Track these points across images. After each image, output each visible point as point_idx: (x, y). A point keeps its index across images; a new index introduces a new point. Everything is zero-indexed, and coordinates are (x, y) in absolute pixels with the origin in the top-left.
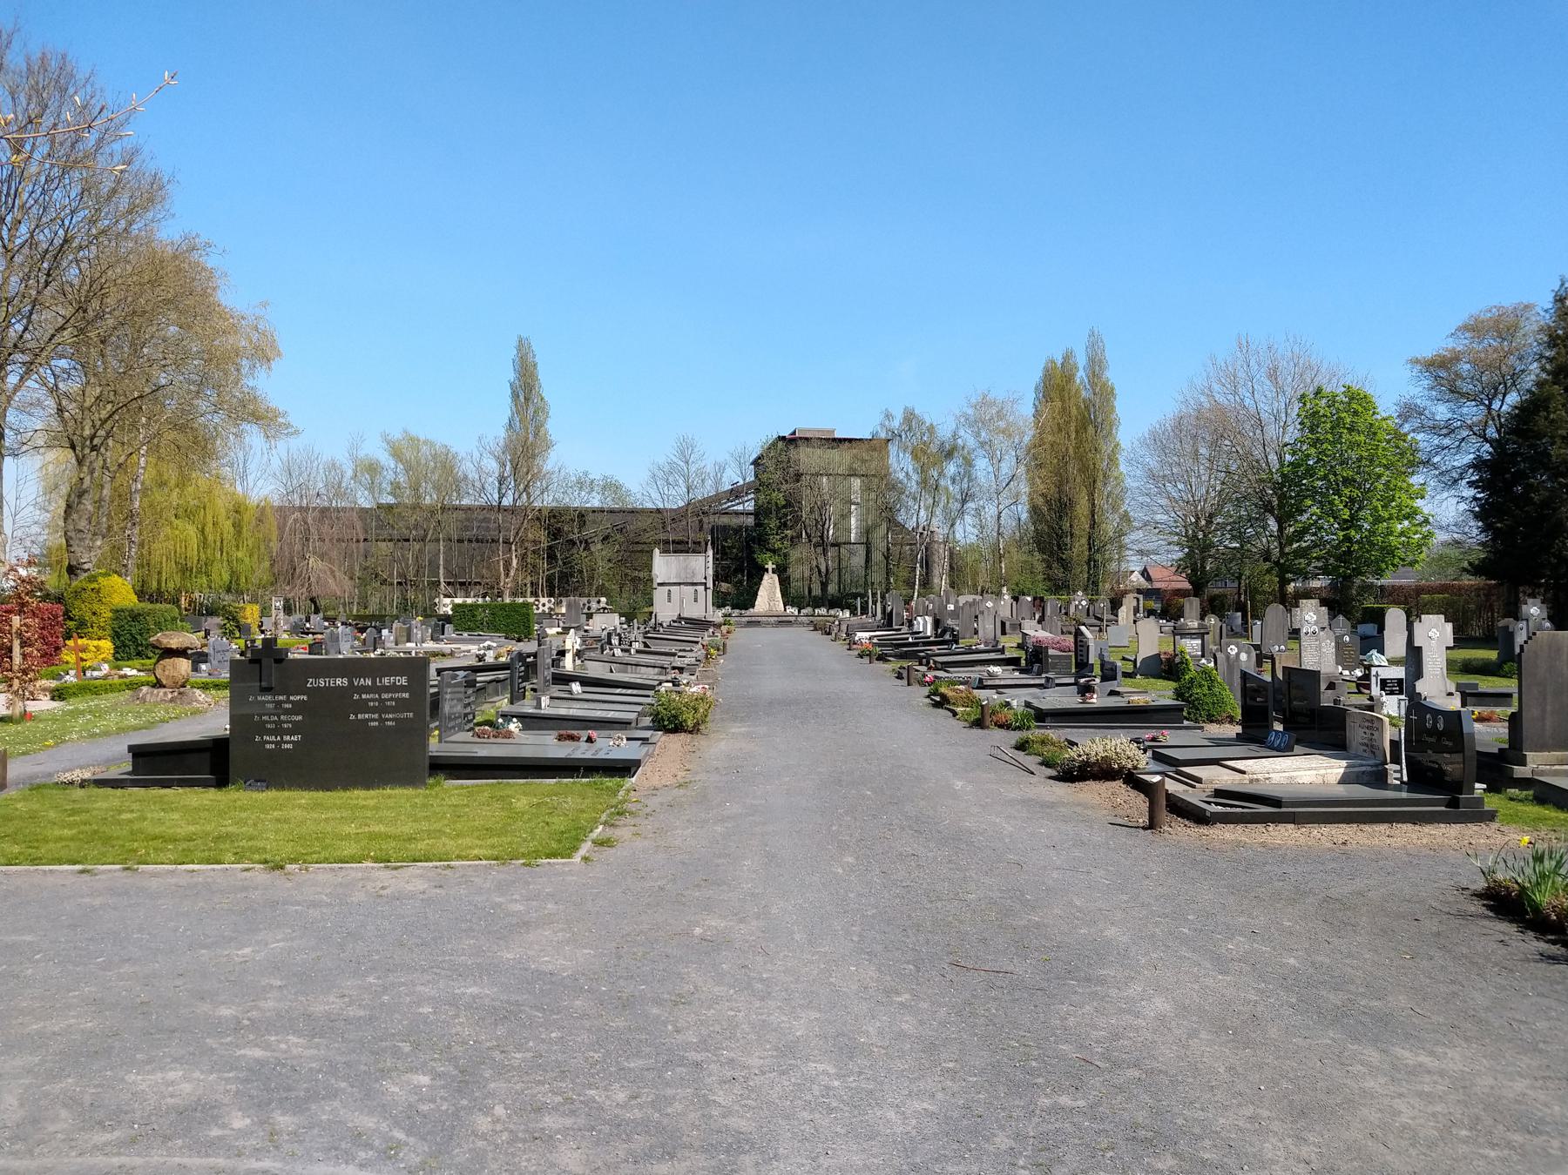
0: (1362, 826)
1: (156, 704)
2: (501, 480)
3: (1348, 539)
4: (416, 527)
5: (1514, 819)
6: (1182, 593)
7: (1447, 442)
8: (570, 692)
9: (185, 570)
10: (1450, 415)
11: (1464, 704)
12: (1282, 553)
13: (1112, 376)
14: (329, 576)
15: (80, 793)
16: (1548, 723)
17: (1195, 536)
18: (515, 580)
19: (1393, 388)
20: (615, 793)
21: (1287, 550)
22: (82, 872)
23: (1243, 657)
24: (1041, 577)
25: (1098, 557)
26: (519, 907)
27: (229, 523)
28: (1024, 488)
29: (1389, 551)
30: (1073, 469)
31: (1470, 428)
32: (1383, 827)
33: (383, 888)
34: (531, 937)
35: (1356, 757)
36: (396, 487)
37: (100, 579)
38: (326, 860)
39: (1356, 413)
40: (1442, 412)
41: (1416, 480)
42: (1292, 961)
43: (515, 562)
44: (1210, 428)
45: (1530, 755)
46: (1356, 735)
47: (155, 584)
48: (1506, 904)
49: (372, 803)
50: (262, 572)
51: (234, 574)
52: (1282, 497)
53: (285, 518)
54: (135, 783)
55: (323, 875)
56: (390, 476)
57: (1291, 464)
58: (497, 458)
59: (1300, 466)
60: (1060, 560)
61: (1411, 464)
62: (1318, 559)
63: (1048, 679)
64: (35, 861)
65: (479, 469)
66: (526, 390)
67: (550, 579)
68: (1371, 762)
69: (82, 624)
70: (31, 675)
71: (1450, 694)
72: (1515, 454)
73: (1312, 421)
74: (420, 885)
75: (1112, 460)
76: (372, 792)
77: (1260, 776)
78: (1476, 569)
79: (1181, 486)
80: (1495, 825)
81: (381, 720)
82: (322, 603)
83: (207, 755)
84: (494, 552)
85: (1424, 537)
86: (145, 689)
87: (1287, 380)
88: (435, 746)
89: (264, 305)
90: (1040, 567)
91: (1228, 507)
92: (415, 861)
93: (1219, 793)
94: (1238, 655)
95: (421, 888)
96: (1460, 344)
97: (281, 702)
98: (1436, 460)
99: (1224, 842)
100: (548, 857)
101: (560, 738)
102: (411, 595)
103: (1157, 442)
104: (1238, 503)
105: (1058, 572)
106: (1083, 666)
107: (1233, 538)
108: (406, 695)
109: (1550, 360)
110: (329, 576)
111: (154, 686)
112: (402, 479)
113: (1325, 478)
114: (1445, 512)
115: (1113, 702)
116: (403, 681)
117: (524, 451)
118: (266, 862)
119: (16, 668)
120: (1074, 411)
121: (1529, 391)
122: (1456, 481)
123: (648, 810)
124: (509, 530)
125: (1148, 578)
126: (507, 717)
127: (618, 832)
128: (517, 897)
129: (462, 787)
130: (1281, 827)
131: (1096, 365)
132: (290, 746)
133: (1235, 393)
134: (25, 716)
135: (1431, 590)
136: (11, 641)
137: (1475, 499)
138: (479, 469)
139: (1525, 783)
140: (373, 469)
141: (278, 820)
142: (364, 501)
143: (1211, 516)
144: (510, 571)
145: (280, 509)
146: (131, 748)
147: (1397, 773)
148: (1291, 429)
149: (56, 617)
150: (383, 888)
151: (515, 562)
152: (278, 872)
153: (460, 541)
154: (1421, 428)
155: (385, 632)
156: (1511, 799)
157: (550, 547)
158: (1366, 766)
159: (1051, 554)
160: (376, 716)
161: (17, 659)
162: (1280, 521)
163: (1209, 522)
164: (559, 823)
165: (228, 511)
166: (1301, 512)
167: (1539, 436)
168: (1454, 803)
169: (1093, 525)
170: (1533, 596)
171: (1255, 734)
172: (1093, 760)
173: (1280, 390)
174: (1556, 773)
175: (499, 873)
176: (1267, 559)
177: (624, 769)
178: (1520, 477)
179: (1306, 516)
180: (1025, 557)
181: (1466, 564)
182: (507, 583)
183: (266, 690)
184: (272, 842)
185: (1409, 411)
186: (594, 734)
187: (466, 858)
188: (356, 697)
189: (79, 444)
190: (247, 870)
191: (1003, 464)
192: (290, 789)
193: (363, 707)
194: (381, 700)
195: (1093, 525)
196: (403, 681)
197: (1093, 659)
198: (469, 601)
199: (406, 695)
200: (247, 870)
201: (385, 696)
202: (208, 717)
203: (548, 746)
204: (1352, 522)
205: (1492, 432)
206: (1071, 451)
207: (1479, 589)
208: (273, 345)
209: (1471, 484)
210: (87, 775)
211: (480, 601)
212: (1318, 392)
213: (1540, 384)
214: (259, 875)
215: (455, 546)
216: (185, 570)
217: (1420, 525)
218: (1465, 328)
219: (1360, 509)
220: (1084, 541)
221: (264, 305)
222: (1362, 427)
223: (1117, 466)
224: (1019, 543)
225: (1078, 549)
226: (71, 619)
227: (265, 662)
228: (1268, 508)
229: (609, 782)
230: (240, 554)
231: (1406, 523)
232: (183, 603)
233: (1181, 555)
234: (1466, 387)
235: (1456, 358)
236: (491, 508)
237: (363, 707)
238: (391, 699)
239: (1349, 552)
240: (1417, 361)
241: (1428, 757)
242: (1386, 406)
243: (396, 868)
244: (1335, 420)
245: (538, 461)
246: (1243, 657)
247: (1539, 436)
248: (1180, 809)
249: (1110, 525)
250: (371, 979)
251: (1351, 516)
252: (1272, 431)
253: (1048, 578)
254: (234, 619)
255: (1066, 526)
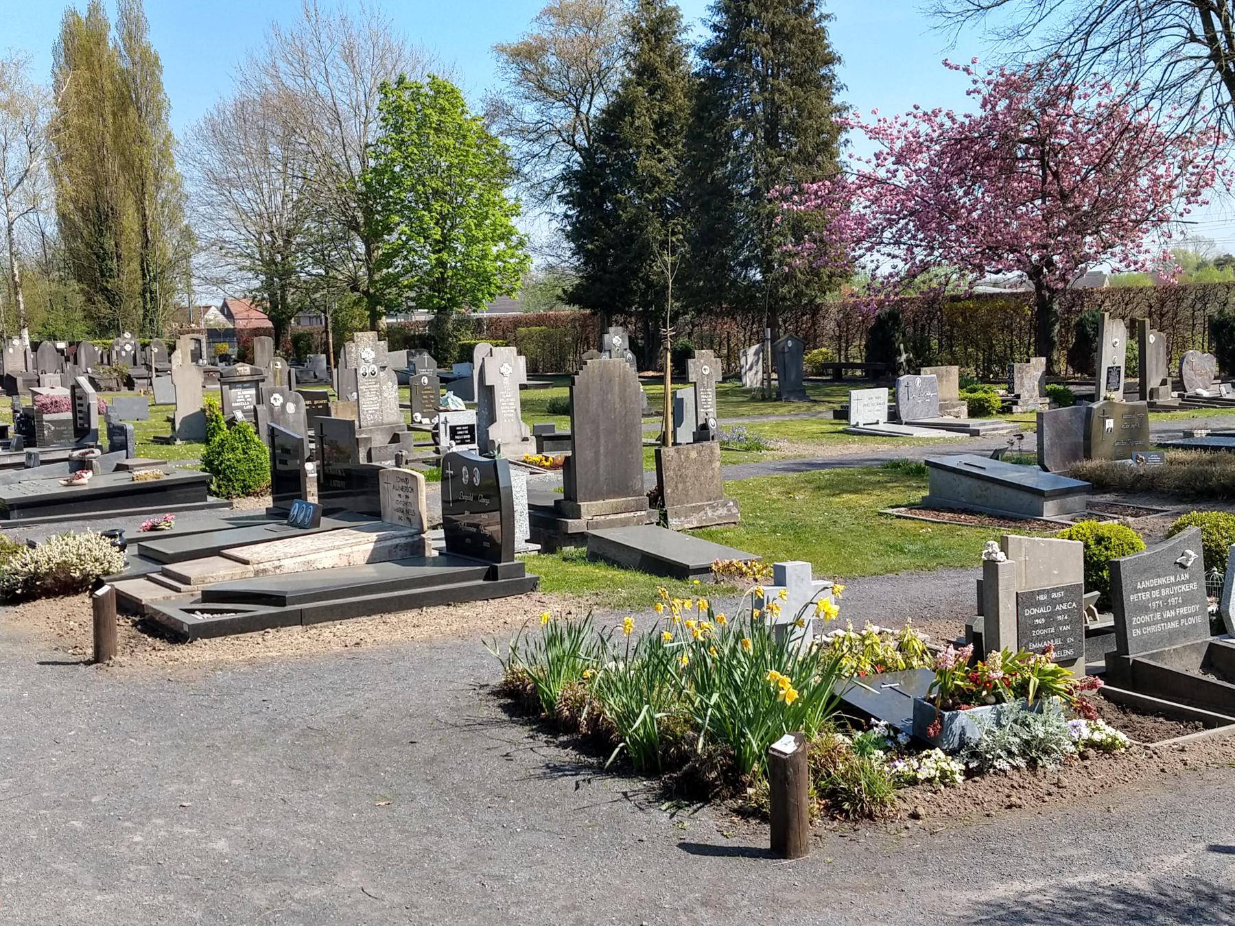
0: (387, 617)
3: (441, 264)
5: (559, 585)
6: (257, 332)
7: (536, 148)
10: (538, 117)
11: (540, 450)
12: (372, 282)
13: (156, 40)
16: (602, 465)
17: (273, 261)
19: (481, 82)
21: (377, 277)
23: (291, 408)
24: (79, 314)
25: (155, 286)
28: (48, 194)
29: (484, 278)
30: (112, 166)
31: (559, 132)
32: (410, 616)
35: (392, 527)
39: (443, 110)
40: (530, 112)
41: (509, 193)
42: (221, 845)
44: (274, 121)
45: (584, 505)
46: (390, 498)
48: (522, 703)
52: (369, 212)
57: (375, 170)
59: (383, 172)
60: (104, 290)
61: (504, 173)
62: (410, 287)
63: (29, 455)
68: (405, 532)
71: (525, 439)
72: (604, 165)
73: (395, 116)
75: (164, 155)
77: (268, 566)
78: (572, 298)
79: (250, 194)
80: (536, 596)
85: (521, 262)
87: (366, 64)
90: (80, 299)
91: (309, 224)
93: (208, 596)
94: (283, 406)
96: (545, 31)
98: (526, 169)
99: (200, 665)
103: (216, 133)
104: (320, 217)
105: (104, 309)
106: (82, 432)
107: (316, 262)
109: (635, 57)
113: (413, 188)
114: (538, 236)
115: (121, 480)
120: (109, 86)
121: (616, 92)
122: (548, 195)
125: (230, 316)
130: (284, 632)
131: (133, 27)
133: (305, 75)
135: (528, 323)
137: (566, 216)
139: (580, 538)
143: (290, 234)
147: (435, 541)
148: (373, 126)
154: (509, 131)
156: (565, 559)
158: (399, 537)
159: (94, 281)
162: (367, 242)
163: (287, 242)
166: (390, 231)
167: (626, 145)
168: (492, 575)
169: (146, 243)
170: (624, 324)
171: (286, 514)
172: (44, 569)
173: (359, 77)
174: (611, 524)
176: (355, 288)
178: (609, 190)
179: (395, 235)
180: (54, 287)
181: (559, 292)
185: (497, 110)
191: (10, 154)
195: (146, 243)
197: (97, 422)
204: (443, 244)
205: (581, 139)
206: (108, 139)
207: (574, 320)
209: (562, 198)
212: (401, 81)
213: (625, 84)
217: (516, 247)
218: (549, 12)
219: (453, 227)
220: (135, 265)
222: (450, 127)
223: (171, 164)
224: (45, 268)
225: (128, 278)
228: (353, 225)
231: (502, 245)
233: (256, 284)
234: (556, 85)
235: (542, 48)
239: (442, 280)
240: (501, 49)
241: (465, 519)
242: (475, 106)
244: (419, 112)
246: (291, 408)
247: (626, 145)
248: (158, 628)
249: (168, 244)
251: (443, 235)
252: (352, 129)
253: (89, 316)
255: (109, 244)
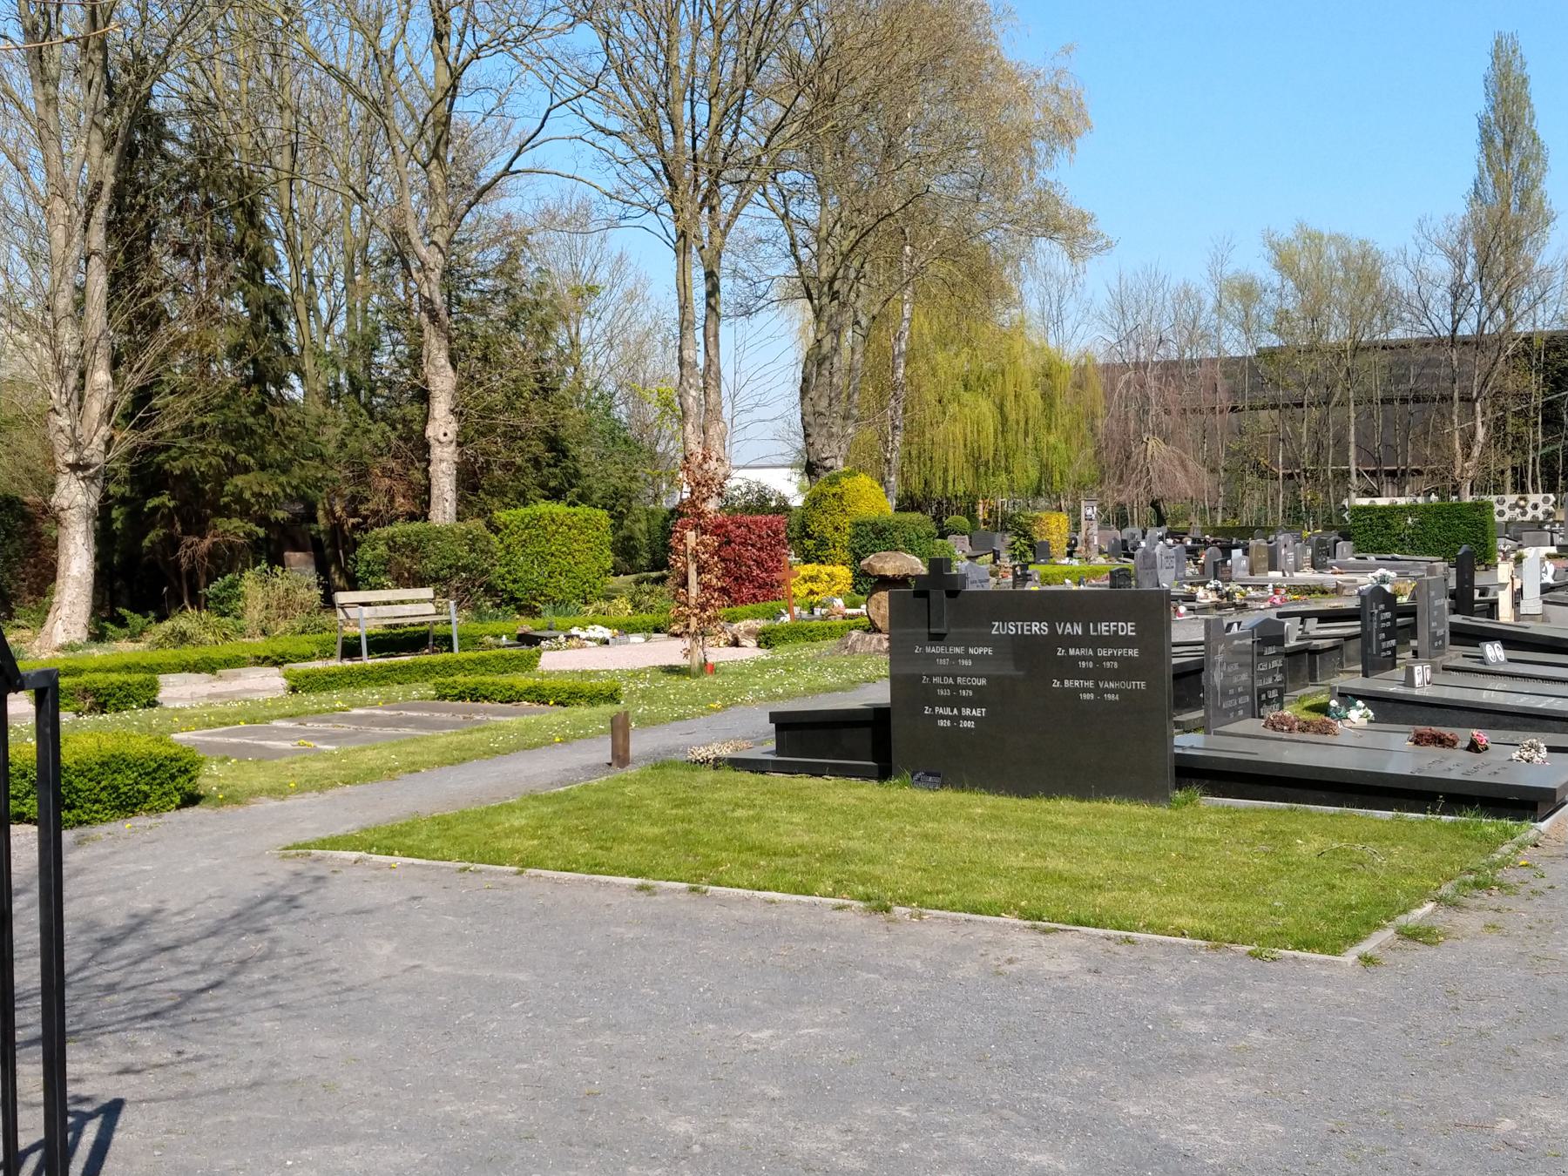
1: (868, 654)
2: (1457, 290)
4: (1314, 381)
8: (1482, 659)
9: (976, 462)
14: (1177, 469)
15: (708, 775)
18: (1483, 463)
20: (1492, 844)
22: (641, 888)
26: (1200, 1027)
27: (1037, 393)
33: (1010, 961)
34: (1192, 1083)
36: (1283, 316)
37: (844, 481)
38: (952, 907)
43: (1481, 433)
47: (940, 487)
49: (1073, 821)
50: (1081, 463)
51: (1045, 468)
53: (1112, 382)
54: (779, 767)
55: (938, 927)
56: (1271, 300)
58: (1452, 254)
64: (595, 867)
65: (1418, 275)
66: (1507, 132)
67: (1548, 462)
69: (822, 543)
70: (710, 612)
74: (1068, 964)
76: (1086, 805)
81: (1097, 690)
82: (1167, 508)
83: (868, 731)
84: (1445, 417)
86: (855, 633)
88: (1188, 743)
89: (1067, 50)
92: (1078, 922)
95: (1066, 968)
97: (957, 657)
100: (1297, 947)
101: (1419, 740)
102: (1306, 494)
108: (1133, 653)
110: (1177, 469)
111: (867, 631)
112: (1290, 304)
116: (1128, 629)
117: (1498, 239)
118: (869, 899)
119: (692, 602)
123: (1540, 885)
124: (1471, 378)
126: (1348, 698)
127: (1460, 919)
128: (1209, 1009)
129: (1228, 810)
132: (970, 724)
134: (706, 668)
136: (686, 565)
138: (1418, 275)
140: (1247, 292)
141: (926, 837)
142: (1234, 345)
144: (1469, 445)
145: (1107, 368)
146: (774, 717)
149: (776, 533)
150: (1010, 961)
151: (1481, 433)
152: (881, 917)
153: (1387, 401)
155: (1237, 553)
157: (1548, 405)
160: (1090, 684)
161: (694, 589)
164: (1354, 890)
165: (1035, 375)
175: (1204, 962)
177: (1526, 804)
182: (1466, 470)
183: (937, 638)
184: (898, 871)
186: (1483, 736)
187: (1162, 930)
188: (1061, 652)
189: (822, 293)
190: (840, 908)
192: (971, 790)
193: (1070, 668)
194: (1098, 660)
196: (1128, 629)
198: (1401, 501)
199: (1133, 653)
200: (840, 908)
201: (1102, 652)
202: (860, 679)
203: (1400, 755)
208: (1081, 115)
210: (726, 752)
211: (1420, 500)
214: (854, 917)
215: (1378, 412)
216: (976, 462)
221: (1067, 50)
226: (810, 537)
227: (934, 595)
229: (1490, 825)
230: (1052, 439)
232: (981, 513)
236: (1440, 341)
237: (1070, 668)
238: (1112, 658)
243: (1046, 932)
245: (1527, 251)
250: (903, 1111)
254: (1026, 535)
